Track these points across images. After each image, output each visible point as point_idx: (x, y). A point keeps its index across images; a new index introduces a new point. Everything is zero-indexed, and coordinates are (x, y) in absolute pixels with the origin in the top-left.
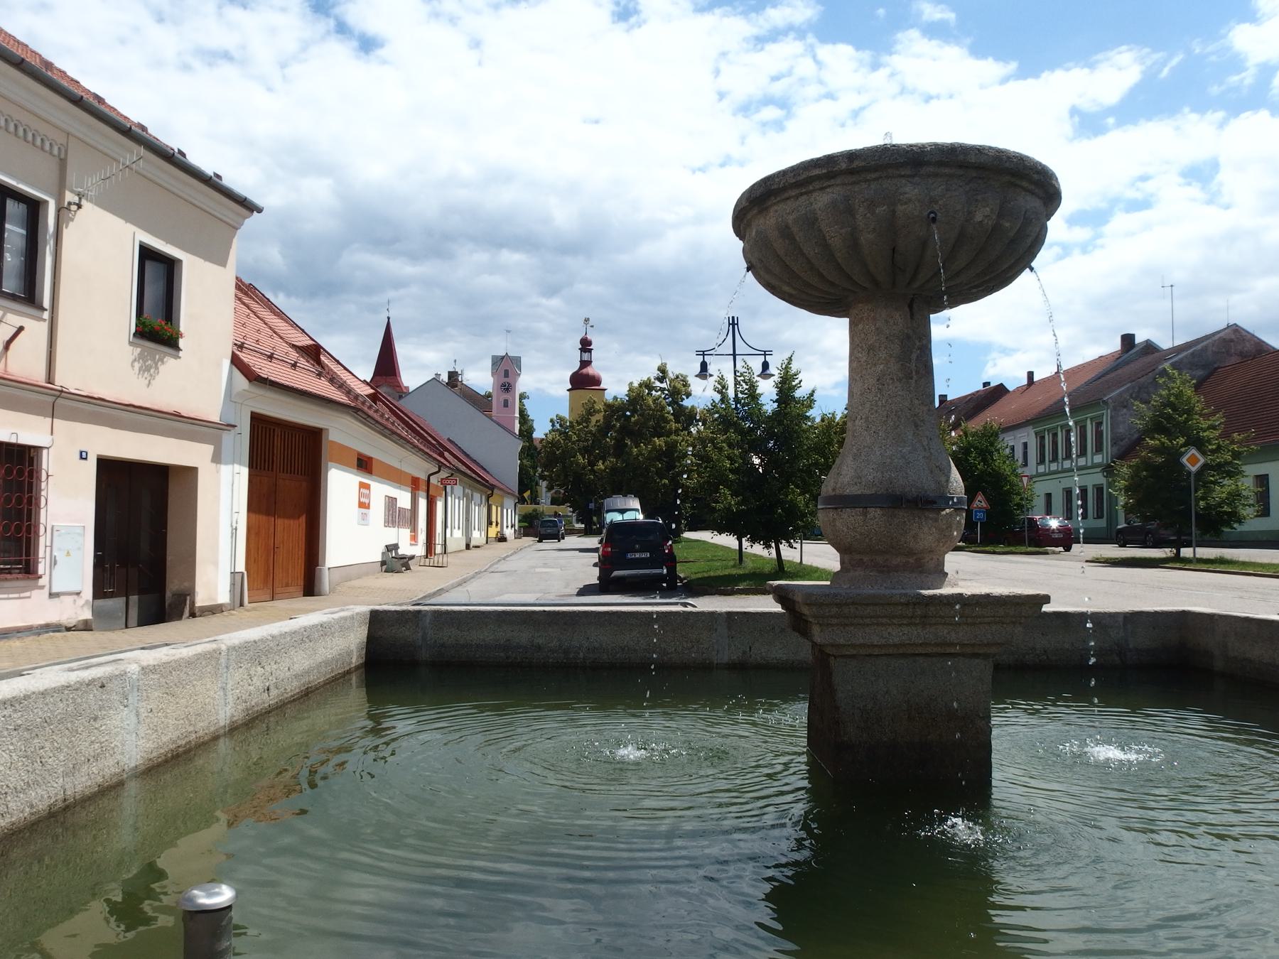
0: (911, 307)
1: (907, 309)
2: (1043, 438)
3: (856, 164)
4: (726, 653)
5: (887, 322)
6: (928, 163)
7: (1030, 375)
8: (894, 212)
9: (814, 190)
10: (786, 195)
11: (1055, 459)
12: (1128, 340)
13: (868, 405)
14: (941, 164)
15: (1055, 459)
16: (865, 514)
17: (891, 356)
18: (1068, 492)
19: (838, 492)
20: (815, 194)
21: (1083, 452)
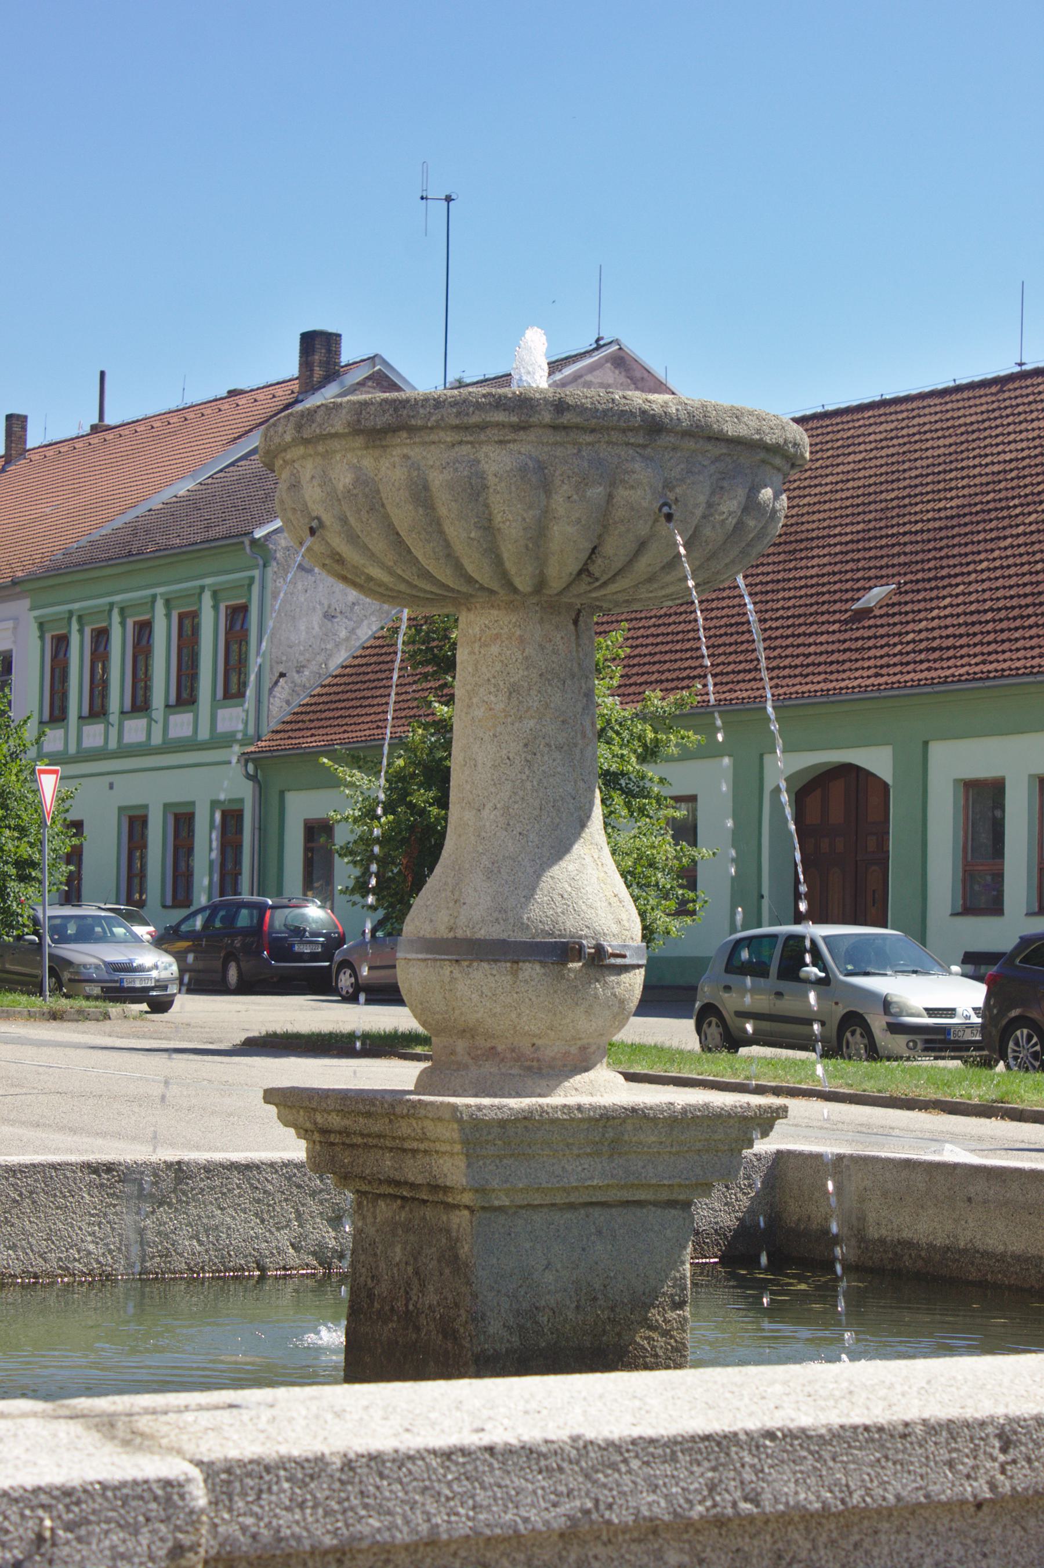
0: (576, 622)
1: (572, 627)
2: (61, 642)
3: (567, 418)
4: (91, 1238)
5: (542, 647)
6: (670, 431)
7: (16, 424)
8: (610, 496)
9: (487, 442)
10: (433, 437)
11: (97, 712)
12: (318, 349)
13: (508, 786)
14: (687, 434)
15: (97, 712)
16: (515, 974)
17: (547, 706)
18: (182, 821)
19: (460, 934)
20: (485, 448)
21: (185, 697)
